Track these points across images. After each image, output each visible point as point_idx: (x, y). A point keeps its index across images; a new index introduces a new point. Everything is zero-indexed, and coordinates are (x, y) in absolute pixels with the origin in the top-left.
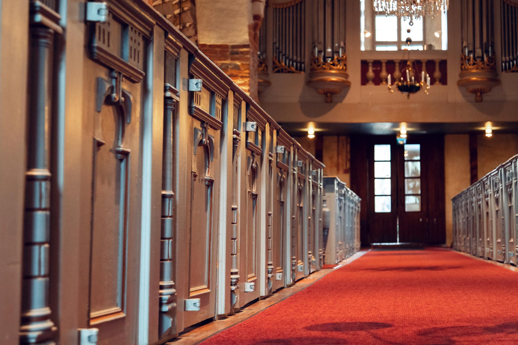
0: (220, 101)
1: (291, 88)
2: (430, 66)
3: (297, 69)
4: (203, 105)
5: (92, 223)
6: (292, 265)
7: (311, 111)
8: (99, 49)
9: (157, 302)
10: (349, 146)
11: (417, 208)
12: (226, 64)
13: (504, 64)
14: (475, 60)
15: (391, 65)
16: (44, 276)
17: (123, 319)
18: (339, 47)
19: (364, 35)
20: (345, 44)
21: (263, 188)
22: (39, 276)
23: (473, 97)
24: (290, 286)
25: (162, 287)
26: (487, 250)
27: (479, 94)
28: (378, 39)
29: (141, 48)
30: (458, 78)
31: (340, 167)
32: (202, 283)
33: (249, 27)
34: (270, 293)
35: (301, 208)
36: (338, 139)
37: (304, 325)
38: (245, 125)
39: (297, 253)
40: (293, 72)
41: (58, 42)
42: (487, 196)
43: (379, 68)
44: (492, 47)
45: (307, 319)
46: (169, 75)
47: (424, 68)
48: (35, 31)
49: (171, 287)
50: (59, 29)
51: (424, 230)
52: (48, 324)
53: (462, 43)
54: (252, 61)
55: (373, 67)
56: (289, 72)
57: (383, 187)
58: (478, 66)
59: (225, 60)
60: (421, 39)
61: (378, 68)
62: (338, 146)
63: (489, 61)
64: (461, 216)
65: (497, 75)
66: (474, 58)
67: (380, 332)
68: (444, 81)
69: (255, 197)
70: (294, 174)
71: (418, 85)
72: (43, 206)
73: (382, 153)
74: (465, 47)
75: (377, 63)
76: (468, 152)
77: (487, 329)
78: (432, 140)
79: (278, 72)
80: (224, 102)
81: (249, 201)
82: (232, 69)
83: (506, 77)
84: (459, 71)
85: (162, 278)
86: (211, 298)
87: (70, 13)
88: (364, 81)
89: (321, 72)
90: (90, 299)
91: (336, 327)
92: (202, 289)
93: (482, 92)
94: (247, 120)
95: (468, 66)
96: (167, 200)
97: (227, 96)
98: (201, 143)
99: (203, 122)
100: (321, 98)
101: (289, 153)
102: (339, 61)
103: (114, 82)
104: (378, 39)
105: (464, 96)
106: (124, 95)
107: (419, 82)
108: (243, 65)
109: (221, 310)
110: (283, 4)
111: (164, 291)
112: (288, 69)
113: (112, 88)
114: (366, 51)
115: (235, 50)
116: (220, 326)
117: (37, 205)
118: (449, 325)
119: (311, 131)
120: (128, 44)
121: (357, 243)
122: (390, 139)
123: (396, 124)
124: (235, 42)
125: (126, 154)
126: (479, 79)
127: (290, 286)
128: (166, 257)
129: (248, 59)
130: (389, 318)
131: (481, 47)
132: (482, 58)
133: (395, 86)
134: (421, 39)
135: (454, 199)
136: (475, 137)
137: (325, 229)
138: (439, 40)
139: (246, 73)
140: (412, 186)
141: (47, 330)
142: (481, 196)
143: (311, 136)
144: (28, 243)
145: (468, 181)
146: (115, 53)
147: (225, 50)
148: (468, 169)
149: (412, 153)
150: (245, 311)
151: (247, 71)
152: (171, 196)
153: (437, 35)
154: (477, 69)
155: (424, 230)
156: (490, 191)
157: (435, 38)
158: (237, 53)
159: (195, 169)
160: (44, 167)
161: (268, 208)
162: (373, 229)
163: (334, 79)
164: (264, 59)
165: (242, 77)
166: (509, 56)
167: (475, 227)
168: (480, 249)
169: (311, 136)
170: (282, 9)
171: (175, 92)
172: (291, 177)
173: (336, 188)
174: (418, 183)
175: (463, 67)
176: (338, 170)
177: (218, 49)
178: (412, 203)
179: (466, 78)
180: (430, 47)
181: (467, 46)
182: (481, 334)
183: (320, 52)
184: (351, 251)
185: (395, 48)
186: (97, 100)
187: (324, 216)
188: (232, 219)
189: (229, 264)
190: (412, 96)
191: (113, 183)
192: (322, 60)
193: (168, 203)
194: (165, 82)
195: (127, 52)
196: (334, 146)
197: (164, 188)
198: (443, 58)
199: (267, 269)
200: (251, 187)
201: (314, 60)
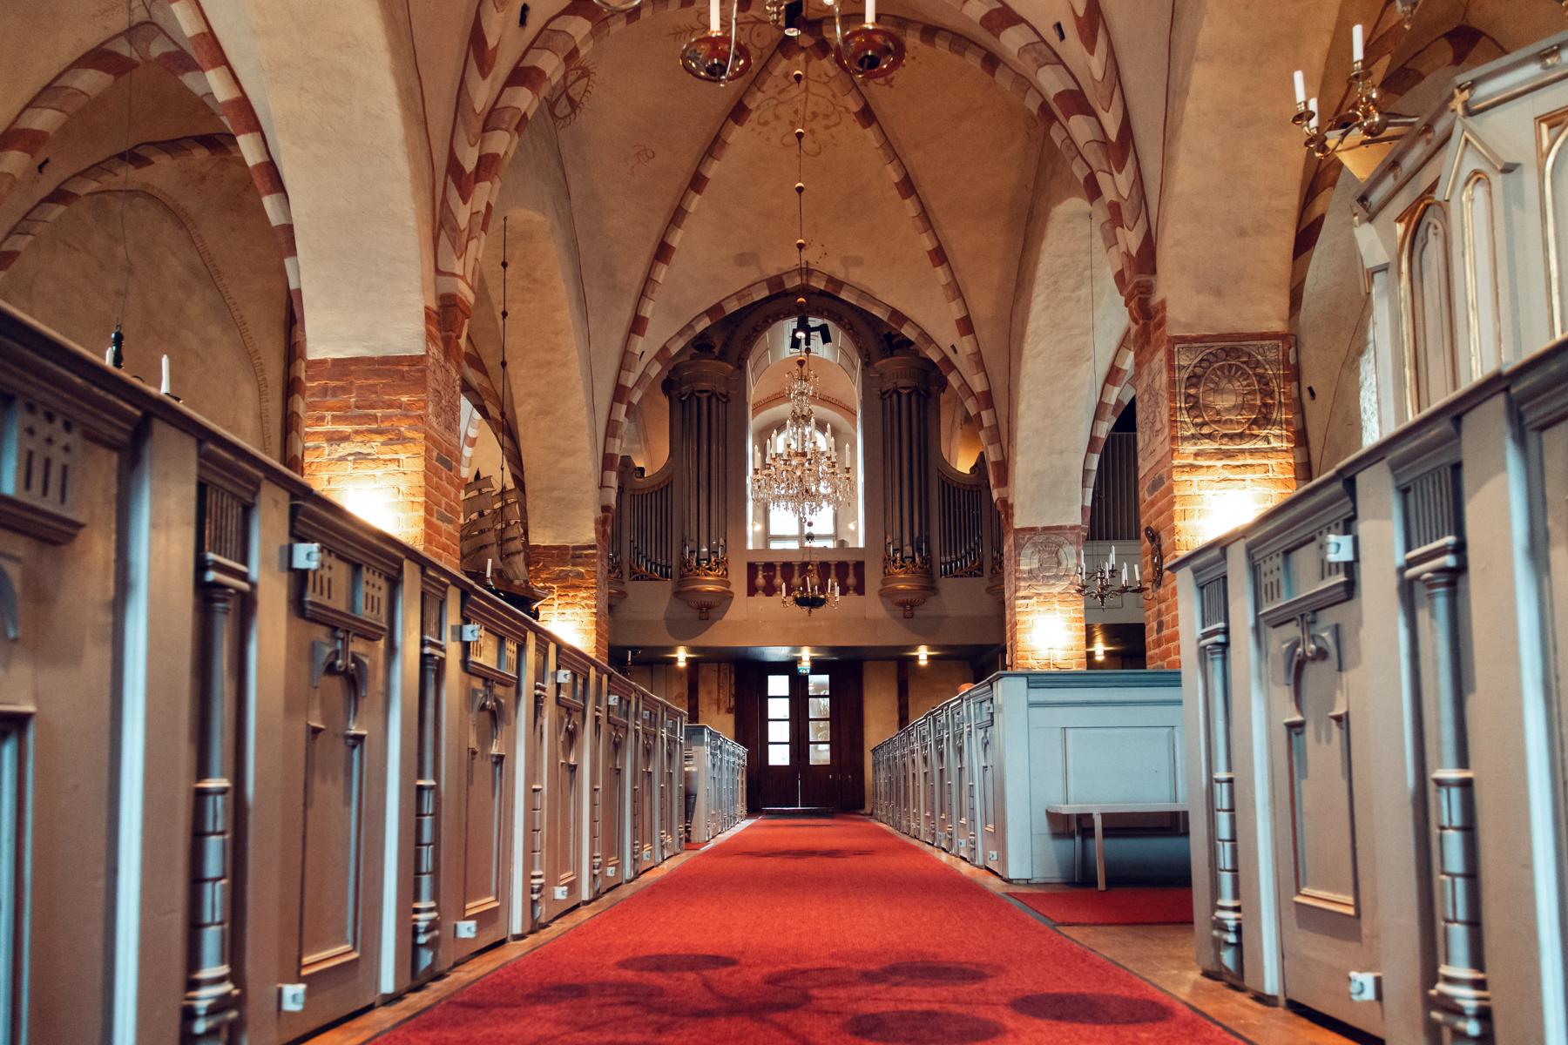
0: (514, 648)
2: (842, 567)
4: (486, 657)
5: (304, 838)
6: (634, 853)
7: (681, 632)
8: (312, 603)
9: (409, 932)
15: (787, 568)
16: (221, 923)
17: (356, 960)
19: (753, 528)
21: (585, 757)
22: (212, 924)
23: (900, 611)
24: (629, 881)
25: (417, 911)
26: (913, 825)
28: (773, 532)
29: (383, 595)
30: (879, 586)
32: (488, 895)
33: (596, 522)
34: (596, 896)
35: (650, 774)
37: (618, 958)
38: (555, 675)
39: (641, 834)
41: (246, 604)
42: (913, 752)
44: (927, 543)
45: (626, 946)
46: (431, 619)
47: (833, 573)
48: (206, 594)
49: (430, 910)
50: (245, 586)
51: (835, 790)
52: (227, 987)
54: (600, 566)
57: (779, 732)
60: (830, 531)
61: (769, 574)
64: (883, 775)
66: (902, 559)
67: (719, 975)
68: (860, 589)
69: (573, 769)
70: (636, 731)
72: (219, 828)
73: (778, 685)
75: (769, 567)
77: (869, 977)
78: (846, 670)
80: (521, 649)
81: (564, 775)
83: (945, 584)
85: (417, 898)
86: (502, 914)
87: (264, 562)
88: (752, 590)
90: (300, 936)
91: (661, 963)
92: (488, 902)
93: (913, 605)
94: (558, 667)
96: (426, 794)
97: (525, 639)
98: (483, 707)
99: (486, 680)
100: (694, 614)
101: (629, 702)
103: (339, 645)
104: (773, 532)
106: (355, 659)
109: (517, 928)
111: (421, 916)
113: (336, 653)
114: (754, 551)
116: (513, 952)
117: (210, 828)
118: (817, 965)
119: (682, 656)
120: (363, 589)
121: (741, 808)
122: (786, 667)
123: (797, 648)
125: (359, 739)
127: (629, 881)
128: (424, 869)
129: (594, 564)
130: (741, 948)
131: (912, 544)
132: (913, 558)
133: (791, 598)
134: (830, 531)
135: (874, 751)
136: (904, 664)
137: (689, 797)
138: (856, 533)
140: (819, 732)
141: (227, 995)
142: (906, 751)
143: (682, 664)
144: (196, 880)
145: (896, 724)
146: (342, 606)
148: (896, 707)
149: (819, 686)
150: (554, 926)
152: (431, 788)
153: (852, 526)
155: (835, 790)
156: (917, 746)
157: (849, 532)
159: (473, 743)
160: (223, 775)
161: (593, 781)
162: (764, 790)
163: (711, 588)
167: (899, 792)
168: (904, 822)
169: (682, 664)
171: (439, 647)
172: (632, 735)
173: (707, 738)
178: (820, 754)
180: (842, 543)
181: (893, 542)
182: (853, 984)
183: (691, 552)
184: (733, 819)
185: (794, 545)
186: (312, 672)
187: (688, 777)
188: (534, 803)
189: (529, 864)
191: (341, 779)
193: (428, 798)
194: (422, 633)
195: (361, 602)
196: (714, 676)
197: (421, 775)
198: (860, 559)
199: (591, 863)
200: (567, 756)
201: (685, 564)
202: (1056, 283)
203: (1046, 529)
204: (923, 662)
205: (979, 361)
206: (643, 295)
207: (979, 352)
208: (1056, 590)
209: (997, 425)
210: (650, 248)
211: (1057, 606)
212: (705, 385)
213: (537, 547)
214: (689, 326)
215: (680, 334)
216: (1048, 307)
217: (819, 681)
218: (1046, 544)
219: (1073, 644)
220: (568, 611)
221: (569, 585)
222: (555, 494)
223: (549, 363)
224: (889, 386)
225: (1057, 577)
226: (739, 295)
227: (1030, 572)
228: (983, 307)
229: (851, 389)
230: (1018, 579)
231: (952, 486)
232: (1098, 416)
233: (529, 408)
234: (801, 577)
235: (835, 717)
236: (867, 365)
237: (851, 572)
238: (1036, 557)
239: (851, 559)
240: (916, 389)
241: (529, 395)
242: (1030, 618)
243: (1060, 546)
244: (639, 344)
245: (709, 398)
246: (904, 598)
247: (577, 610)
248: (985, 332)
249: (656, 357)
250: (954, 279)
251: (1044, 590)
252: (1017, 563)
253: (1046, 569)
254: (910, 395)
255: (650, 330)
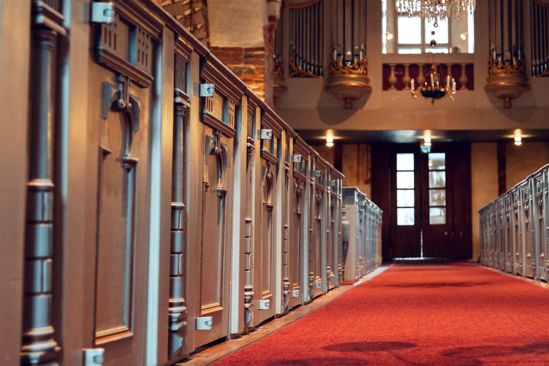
0: (233, 107)
1: (308, 94)
2: (456, 70)
3: (314, 73)
4: (216, 112)
5: (97, 236)
6: (310, 281)
7: (330, 118)
8: (105, 51)
9: (166, 320)
10: (369, 155)
11: (442, 221)
12: (239, 68)
13: (534, 68)
14: (504, 64)
15: (414, 69)
16: (47, 293)
17: (130, 338)
18: (360, 49)
19: (386, 37)
20: (365, 46)
21: (279, 200)
22: (42, 293)
23: (501, 103)
24: (307, 303)
25: (171, 305)
26: (516, 265)
27: (507, 100)
28: (400, 41)
29: (149, 51)
30: (485, 83)
31: (361, 177)
32: (214, 301)
33: (264, 28)
34: (287, 311)
35: (319, 221)
36: (359, 147)
37: (322, 345)
38: (260, 133)
39: (315, 269)
40: (310, 77)
41: (62, 45)
42: (516, 208)
43: (401, 73)
44: (522, 50)
45: (325, 339)
46: (179, 80)
47: (449, 72)
48: (37, 33)
49: (181, 304)
50: (62, 31)
51: (450, 244)
52: (51, 344)
53: (490, 46)
54: (267, 64)
55: (396, 71)
56: (306, 76)
57: (406, 198)
58: (507, 70)
59: (238, 64)
60: (446, 41)
61: (400, 73)
62: (358, 155)
63: (518, 65)
64: (489, 229)
65: (526, 80)
66: (503, 62)
67: (403, 352)
68: (470, 86)
69: (270, 209)
70: (311, 185)
71: (443, 90)
72: (46, 218)
73: (405, 162)
74: (493, 50)
75: (400, 67)
76: (496, 161)
77: (517, 350)
78: (458, 148)
79: (295, 76)
80: (238, 109)
81: (264, 213)
82: (246, 73)
83: (536, 82)
84: (486, 75)
85: (171, 295)
86: (224, 317)
87: (74, 13)
88: (386, 86)
89: (341, 77)
90: (95, 317)
91: (356, 347)
92: (214, 306)
93: (511, 97)
94: (262, 127)
95: (496, 70)
96: (177, 212)
97: (240, 101)
98: (213, 152)
99: (215, 130)
100: (340, 104)
101: (307, 162)
102: (359, 64)
103: (121, 87)
104: (400, 41)
105: (492, 102)
106: (131, 100)
107: (444, 87)
108: (257, 68)
109: (235, 329)
110: (300, 4)
111: (174, 309)
112: (306, 74)
113: (118, 94)
114: (388, 55)
115: (250, 53)
116: (233, 346)
117: (39, 218)
118: (476, 345)
119: (330, 139)
120: (136, 47)
121: (378, 258)
122: (413, 147)
123: (420, 132)
124: (249, 44)
125: (133, 164)
126: (508, 84)
127: (307, 303)
128: (176, 273)
129: (262, 63)
130: (413, 337)
131: (510, 50)
132: (511, 61)
133: (418, 91)
134: (446, 41)
135: (481, 212)
136: (504, 145)
137: (345, 243)
138: (466, 43)
139: (260, 78)
140: (436, 198)
141: (50, 350)
142: (510, 208)
143: (330, 144)
144: (30, 258)
145: (497, 192)
146: (122, 56)
147: (239, 53)
148: (496, 179)
149: (437, 163)
150: (260, 330)
151: (262, 76)
152: (181, 208)
153: (463, 37)
154: (506, 73)
155: (450, 244)
156: (519, 203)
157: (461, 40)
158: (251, 56)
159: (206, 180)
160: (46, 177)
161: (284, 221)
162: (395, 243)
163: (354, 84)
164: (280, 63)
165: (257, 82)
166: (539, 59)
167: (504, 241)
168: (508, 264)
169: (330, 144)
170: (299, 9)
171: (185, 98)
172: (308, 188)
173: (356, 200)
174: (443, 194)
175: (491, 71)
176: (358, 180)
177: (231, 52)
178: (437, 216)
179: (494, 82)
180: (456, 49)
181: (495, 49)
182: (510, 354)
183: (339, 55)
184: (372, 267)
185: (418, 51)
186: (103, 106)
187: (344, 229)
188: (246, 232)
189: (243, 280)
190: (437, 101)
191: (120, 194)
192: (341, 64)
193: (178, 215)
194: (175, 87)
195: (134, 55)
196: (354, 155)
197: (174, 199)
198: (470, 61)
199: (283, 285)
200: (266, 198)
201: (333, 64)
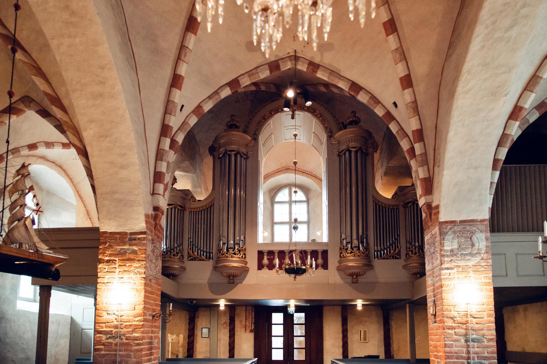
2: (314, 254)
10: (253, 313)
11: (303, 358)
15: (282, 254)
20: (245, 238)
23: (350, 279)
27: (355, 277)
30: (337, 265)
31: (247, 328)
36: (246, 308)
40: (203, 260)
53: (341, 236)
56: (200, 260)
57: (278, 342)
61: (269, 258)
62: (246, 314)
65: (370, 262)
68: (325, 266)
71: (304, 267)
73: (277, 318)
75: (271, 253)
76: (340, 319)
78: (314, 311)
79: (192, 260)
82: (130, 253)
83: (378, 264)
84: (338, 258)
88: (260, 267)
95: (344, 254)
100: (225, 280)
102: (239, 251)
107: (305, 265)
112: (200, 258)
115: (133, 236)
119: (222, 303)
122: (283, 309)
123: (288, 300)
129: (145, 245)
131: (358, 239)
136: (345, 309)
139: (142, 257)
140: (299, 342)
143: (222, 308)
151: (144, 255)
158: (135, 239)
163: (235, 265)
165: (139, 260)
166: (380, 246)
169: (222, 308)
174: (303, 339)
175: (342, 255)
176: (246, 330)
177: (118, 236)
178: (299, 355)
183: (224, 244)
190: (298, 278)
192: (225, 251)
196: (243, 313)
198: (325, 248)
201: (220, 250)
202: (494, 23)
203: (462, 222)
204: (359, 308)
205: (415, 107)
206: (179, 58)
207: (415, 102)
208: (471, 263)
209: (425, 153)
210: (181, 21)
211: (472, 274)
212: (233, 147)
213: (105, 233)
214: (216, 92)
215: (210, 97)
216: (483, 47)
217: (300, 317)
218: (462, 232)
219: (485, 301)
220: (126, 276)
221: (126, 258)
222: (117, 196)
223: (101, 95)
224: (344, 147)
225: (471, 254)
226: (250, 73)
227: (452, 251)
228: (421, 67)
229: (318, 162)
230: (442, 256)
231: (380, 205)
232: (500, 144)
233: (92, 132)
234: (290, 261)
235: (307, 336)
236: (330, 136)
237: (320, 256)
238: (456, 241)
239: (320, 249)
240: (360, 149)
241: (91, 121)
242: (452, 282)
243: (473, 233)
244: (178, 96)
245: (236, 155)
246: (353, 271)
247: (132, 275)
248: (420, 87)
249: (193, 112)
250: (401, 46)
251: (462, 263)
252: (442, 245)
253: (463, 249)
254: (356, 152)
255: (186, 84)
